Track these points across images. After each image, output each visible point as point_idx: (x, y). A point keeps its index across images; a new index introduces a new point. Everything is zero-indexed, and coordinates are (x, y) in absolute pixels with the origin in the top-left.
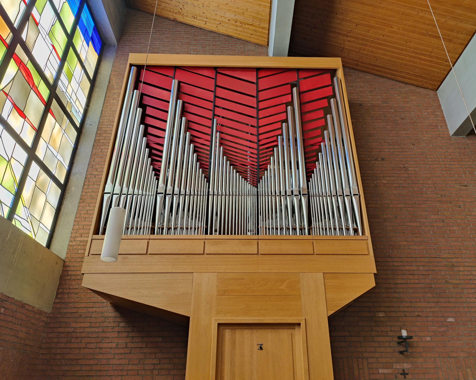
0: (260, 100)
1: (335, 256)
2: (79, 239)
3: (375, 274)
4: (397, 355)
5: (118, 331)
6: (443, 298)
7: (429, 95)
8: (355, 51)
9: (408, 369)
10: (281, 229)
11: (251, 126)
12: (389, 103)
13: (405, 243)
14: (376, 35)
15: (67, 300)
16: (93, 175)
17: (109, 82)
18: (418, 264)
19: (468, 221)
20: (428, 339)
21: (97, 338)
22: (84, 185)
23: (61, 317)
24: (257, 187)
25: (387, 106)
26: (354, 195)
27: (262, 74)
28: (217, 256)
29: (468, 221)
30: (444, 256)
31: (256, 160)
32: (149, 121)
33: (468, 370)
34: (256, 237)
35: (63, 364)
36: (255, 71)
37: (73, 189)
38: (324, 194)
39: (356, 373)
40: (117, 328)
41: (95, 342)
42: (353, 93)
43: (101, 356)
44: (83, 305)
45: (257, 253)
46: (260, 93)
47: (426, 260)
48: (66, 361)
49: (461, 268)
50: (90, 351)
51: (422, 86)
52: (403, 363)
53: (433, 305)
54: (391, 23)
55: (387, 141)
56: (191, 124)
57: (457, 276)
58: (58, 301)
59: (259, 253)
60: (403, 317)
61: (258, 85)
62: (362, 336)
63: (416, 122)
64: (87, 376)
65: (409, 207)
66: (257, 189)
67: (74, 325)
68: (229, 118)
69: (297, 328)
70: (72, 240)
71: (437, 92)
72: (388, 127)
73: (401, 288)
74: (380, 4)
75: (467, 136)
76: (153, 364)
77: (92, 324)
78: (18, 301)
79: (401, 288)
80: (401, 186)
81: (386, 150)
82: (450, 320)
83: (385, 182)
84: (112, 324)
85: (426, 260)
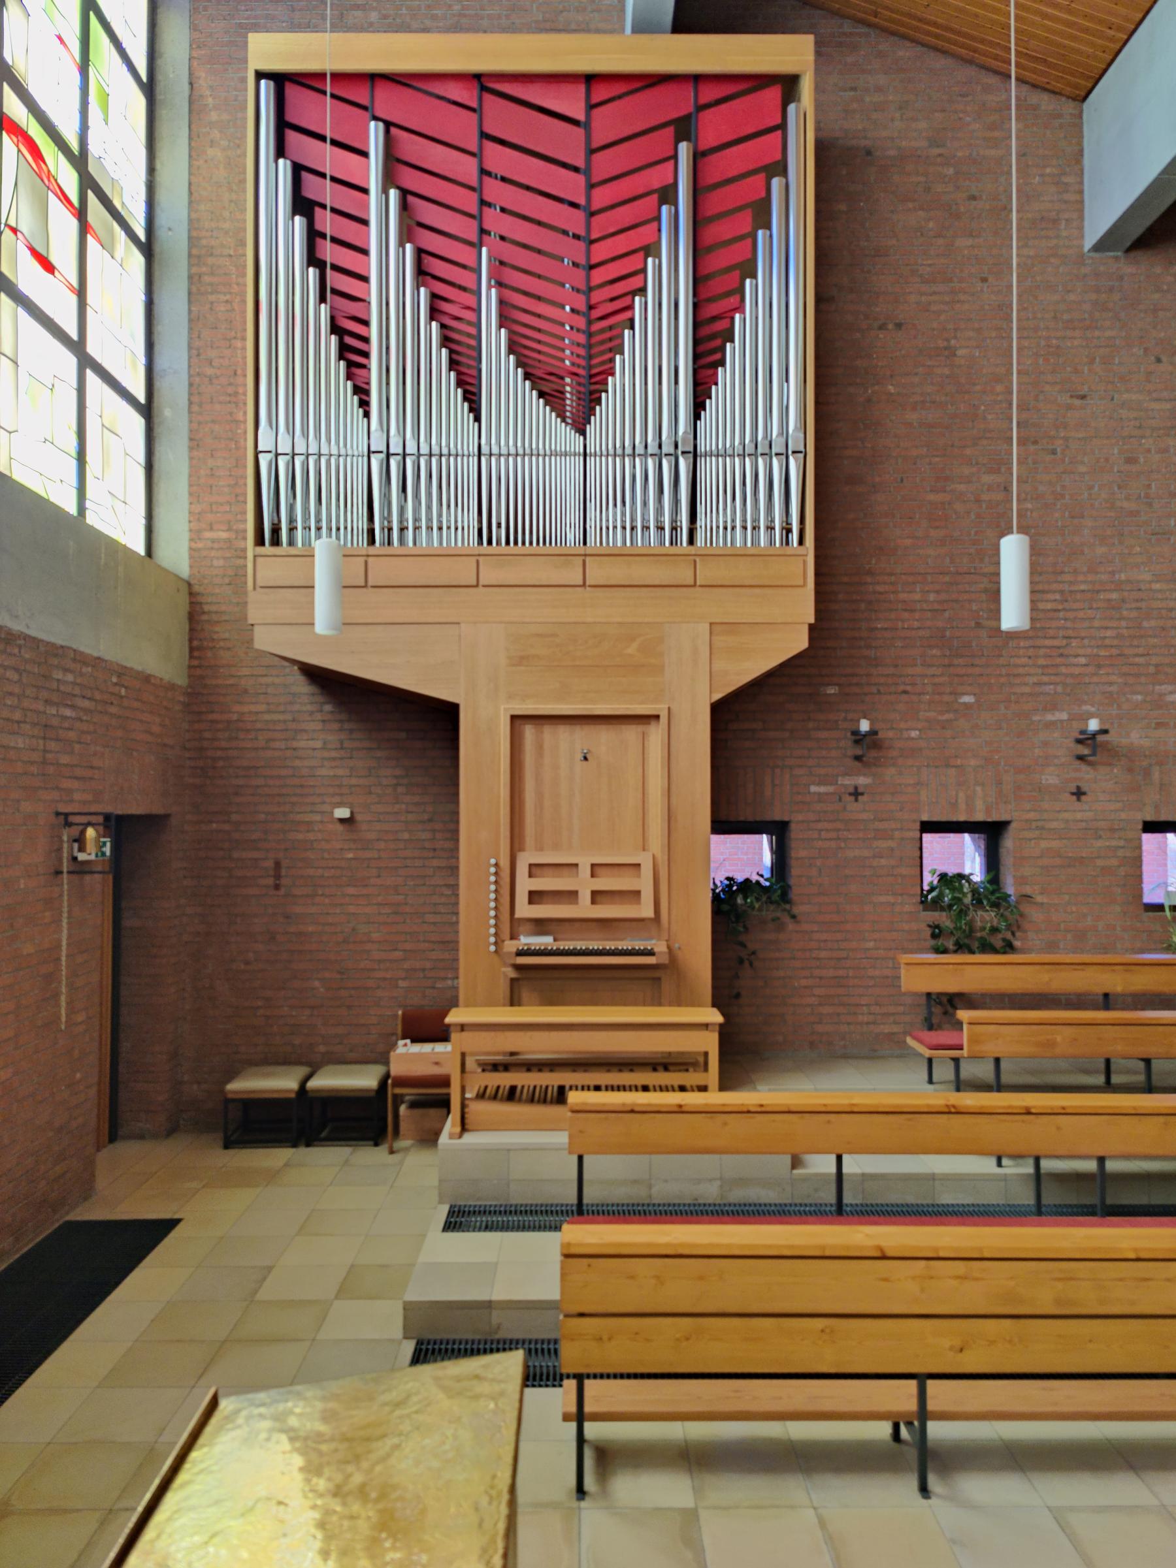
0: (595, 180)
2: (208, 535)
6: (962, 656)
7: (1060, 116)
9: (866, 786)
13: (908, 542)
16: (206, 376)
17: (191, 84)
19: (1063, 487)
20: (914, 734)
22: (191, 403)
24: (583, 432)
27: (601, 92)
29: (1063, 487)
33: (978, 789)
37: (167, 412)
39: (768, 792)
43: (297, 763)
50: (277, 754)
51: (1048, 86)
53: (939, 671)
55: (918, 270)
56: (428, 261)
58: (196, 663)
65: (937, 456)
66: (585, 439)
67: (237, 708)
69: (653, 723)
71: (1086, 105)
72: (931, 225)
75: (1129, 250)
78: (138, 673)
84: (309, 708)
85: (947, 579)
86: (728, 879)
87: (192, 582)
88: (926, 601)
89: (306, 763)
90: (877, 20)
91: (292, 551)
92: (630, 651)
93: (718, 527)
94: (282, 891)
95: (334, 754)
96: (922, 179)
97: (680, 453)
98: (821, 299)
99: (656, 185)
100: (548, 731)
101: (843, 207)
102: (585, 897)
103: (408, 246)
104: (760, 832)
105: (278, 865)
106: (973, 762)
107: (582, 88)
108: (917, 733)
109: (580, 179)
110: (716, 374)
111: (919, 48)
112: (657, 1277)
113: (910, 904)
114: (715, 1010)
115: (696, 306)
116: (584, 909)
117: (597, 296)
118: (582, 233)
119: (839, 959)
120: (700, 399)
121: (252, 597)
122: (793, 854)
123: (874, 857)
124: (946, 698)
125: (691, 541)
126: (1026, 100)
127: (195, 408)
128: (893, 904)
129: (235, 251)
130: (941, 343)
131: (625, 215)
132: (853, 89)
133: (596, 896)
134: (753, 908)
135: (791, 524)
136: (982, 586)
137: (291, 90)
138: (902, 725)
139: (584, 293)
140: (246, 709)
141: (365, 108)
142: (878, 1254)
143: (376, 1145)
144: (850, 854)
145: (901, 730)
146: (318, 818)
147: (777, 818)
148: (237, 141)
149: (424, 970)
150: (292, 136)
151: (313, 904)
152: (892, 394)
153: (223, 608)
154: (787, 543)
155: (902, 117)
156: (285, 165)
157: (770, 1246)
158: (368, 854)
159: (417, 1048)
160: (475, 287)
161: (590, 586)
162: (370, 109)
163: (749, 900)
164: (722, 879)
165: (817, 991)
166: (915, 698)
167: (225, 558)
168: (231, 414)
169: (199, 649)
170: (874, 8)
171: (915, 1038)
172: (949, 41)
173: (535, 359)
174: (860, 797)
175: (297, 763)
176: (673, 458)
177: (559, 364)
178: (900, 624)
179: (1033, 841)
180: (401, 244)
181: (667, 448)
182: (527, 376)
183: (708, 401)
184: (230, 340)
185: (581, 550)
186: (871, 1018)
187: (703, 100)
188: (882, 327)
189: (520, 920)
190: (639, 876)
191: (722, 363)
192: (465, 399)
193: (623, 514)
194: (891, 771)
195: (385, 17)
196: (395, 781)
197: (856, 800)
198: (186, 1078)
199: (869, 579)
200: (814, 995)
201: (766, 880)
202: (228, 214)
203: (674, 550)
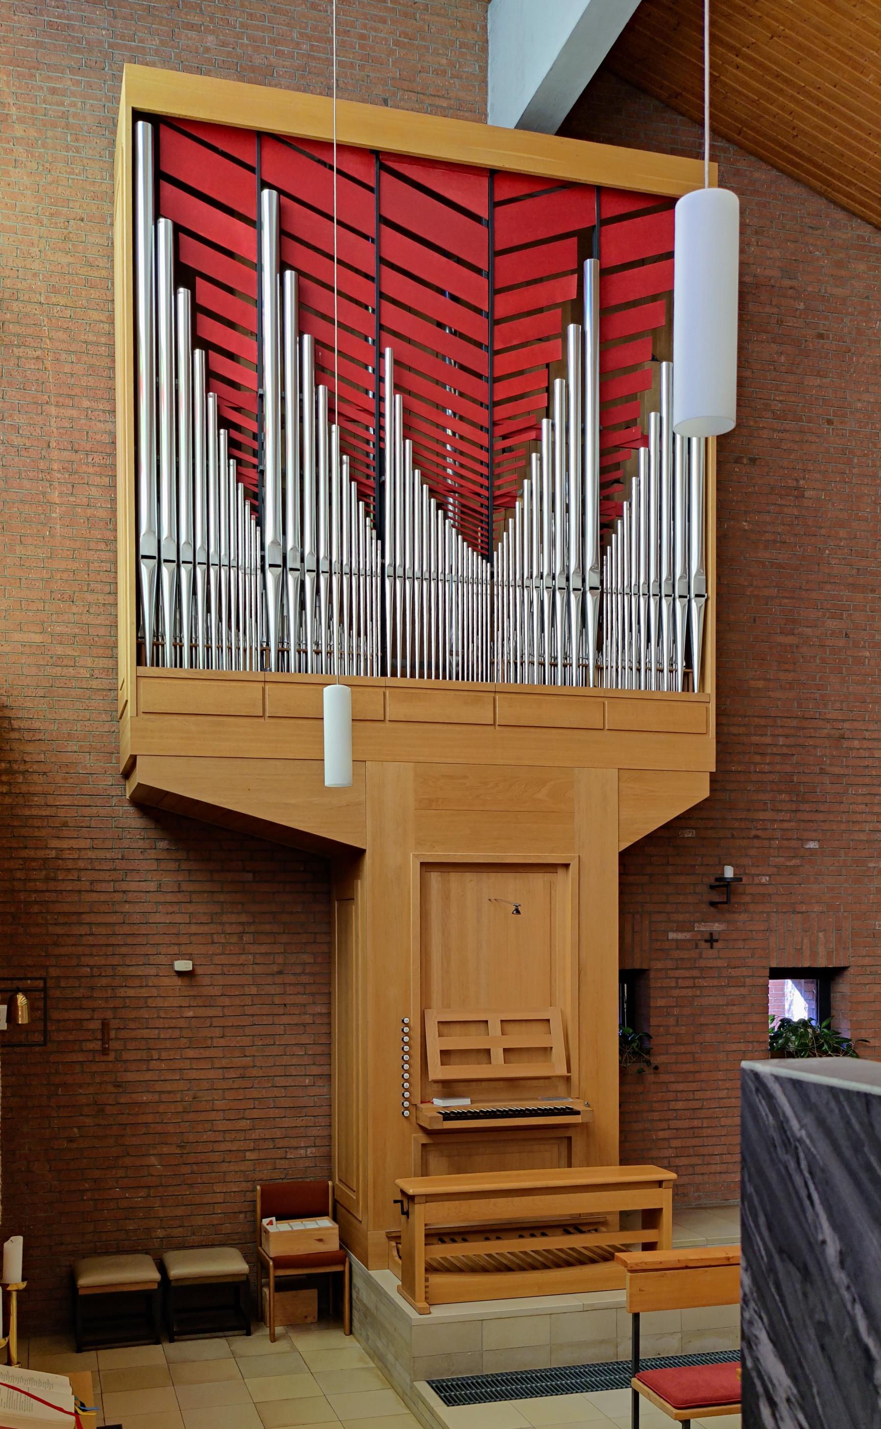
0: (498, 286)
1: (645, 734)
2: (18, 636)
3: (711, 773)
4: (705, 908)
6: (807, 802)
8: (747, 97)
9: (719, 932)
12: (796, 278)
13: (761, 684)
14: (814, 77)
15: (24, 789)
18: (776, 732)
20: (765, 879)
23: (21, 826)
24: (488, 557)
25: (791, 288)
26: (697, 596)
27: (504, 191)
30: (829, 716)
31: (486, 483)
33: (821, 935)
35: (50, 922)
36: (485, 176)
41: (111, 878)
43: (127, 908)
44: (65, 801)
45: (492, 723)
47: (795, 723)
48: (56, 917)
49: (856, 744)
50: (103, 897)
53: (787, 816)
54: (865, 63)
57: (844, 759)
62: (647, 875)
63: (850, 350)
66: (492, 566)
67: (55, 843)
69: (561, 871)
72: (783, 359)
74: (854, 8)
77: (96, 842)
80: (779, 540)
81: (765, 434)
82: (812, 845)
83: (747, 528)
84: (141, 844)
85: (795, 723)
88: (776, 745)
89: (138, 908)
90: (739, 138)
94: (111, 1057)
95: (169, 898)
96: (775, 310)
100: (454, 877)
102: (498, 1055)
105: (105, 1024)
106: (817, 908)
107: (485, 182)
108: (767, 878)
111: (774, 172)
116: (498, 1068)
123: (727, 1005)
124: (794, 844)
126: (869, 241)
129: (47, 298)
130: (791, 483)
136: (826, 731)
138: (754, 871)
140: (65, 844)
141: (252, 169)
143: (249, 1334)
144: (705, 1001)
145: (753, 875)
146: (153, 971)
149: (273, 1139)
151: (148, 1070)
152: (745, 530)
153: (37, 725)
155: (758, 243)
159: (284, 1226)
165: (675, 1143)
166: (766, 843)
167: (38, 666)
168: (44, 494)
170: (740, 126)
172: (808, 172)
174: (715, 944)
175: (127, 908)
178: (752, 768)
179: (867, 986)
180: (300, 333)
184: (41, 405)
186: (724, 1167)
187: (608, 213)
188: (738, 461)
194: (743, 917)
195: (224, 44)
196: (240, 929)
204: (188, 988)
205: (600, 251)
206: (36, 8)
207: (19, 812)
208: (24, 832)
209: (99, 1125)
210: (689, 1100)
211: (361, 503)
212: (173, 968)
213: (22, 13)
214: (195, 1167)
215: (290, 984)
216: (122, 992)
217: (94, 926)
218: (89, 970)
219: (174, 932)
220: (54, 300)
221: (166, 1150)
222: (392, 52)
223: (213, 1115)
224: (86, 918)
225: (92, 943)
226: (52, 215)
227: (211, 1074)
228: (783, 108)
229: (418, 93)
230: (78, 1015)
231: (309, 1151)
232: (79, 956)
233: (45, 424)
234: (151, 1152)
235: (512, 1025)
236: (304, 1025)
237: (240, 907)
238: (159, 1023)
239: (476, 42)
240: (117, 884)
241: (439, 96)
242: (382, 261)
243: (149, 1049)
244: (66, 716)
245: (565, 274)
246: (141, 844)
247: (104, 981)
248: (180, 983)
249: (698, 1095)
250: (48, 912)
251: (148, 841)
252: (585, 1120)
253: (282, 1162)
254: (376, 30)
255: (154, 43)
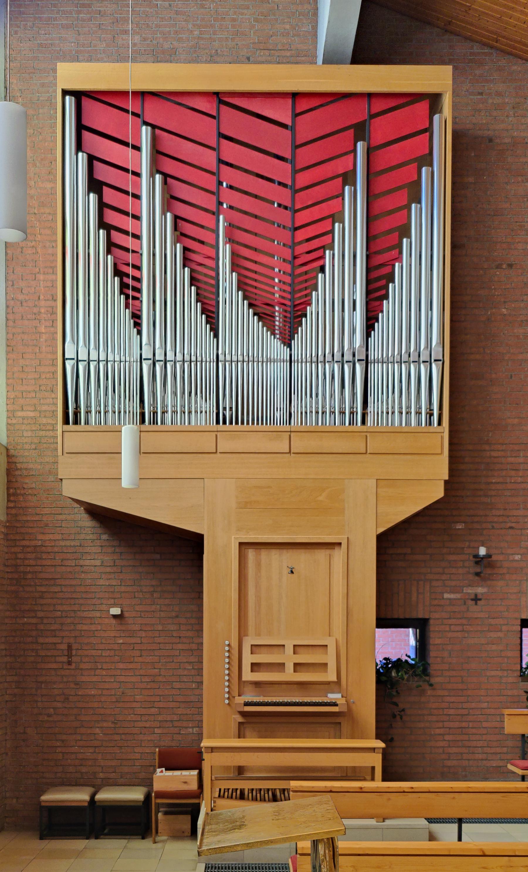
2: (20, 414)
4: (471, 577)
5: (101, 545)
9: (482, 594)
10: (323, 413)
11: (280, 183)
13: (516, 421)
15: (23, 505)
16: (18, 300)
20: (517, 557)
21: (74, 554)
22: (7, 320)
24: (290, 346)
28: (234, 455)
32: (112, 218)
34: (287, 428)
35: (38, 584)
36: (290, 98)
38: (391, 359)
39: (414, 598)
40: (99, 541)
42: (480, 111)
46: (298, 151)
50: (69, 569)
52: (476, 586)
55: (524, 226)
58: (12, 505)
59: (292, 452)
60: (489, 529)
61: (295, 130)
64: (71, 598)
66: (291, 350)
67: (40, 537)
68: (238, 146)
69: (337, 549)
70: (11, 415)
73: (494, 490)
76: (152, 585)
79: (494, 490)
81: (520, 246)
83: (505, 313)
84: (91, 536)
86: (385, 659)
87: (9, 448)
91: (88, 428)
92: (320, 498)
93: (382, 412)
94: (73, 666)
95: (108, 570)
97: (356, 361)
98: (454, 246)
99: (341, 171)
100: (264, 553)
101: (471, 179)
102: (290, 667)
103: (169, 215)
104: (407, 627)
105: (70, 647)
109: (288, 167)
110: (382, 305)
112: (353, 866)
113: (513, 677)
114: (379, 741)
115: (368, 257)
117: (300, 249)
118: (289, 205)
119: (462, 715)
120: (371, 322)
121: (61, 459)
122: (432, 641)
125: (363, 422)
127: (11, 323)
128: (501, 677)
131: (318, 192)
132: (481, 94)
133: (297, 666)
134: (403, 679)
135: (433, 410)
137: (86, 103)
139: (290, 247)
140: (47, 537)
142: (481, 854)
143: (143, 838)
146: (98, 614)
147: (421, 616)
148: (40, 130)
149: (172, 721)
150: (86, 134)
153: (31, 466)
154: (430, 424)
155: (514, 114)
156: (83, 156)
157: (418, 849)
158: (133, 640)
160: (213, 243)
161: (293, 453)
162: (141, 117)
163: (400, 674)
164: (381, 659)
165: (447, 737)
169: (14, 495)
170: (495, 37)
171: (512, 764)
173: (253, 293)
174: (479, 602)
176: (351, 364)
177: (272, 297)
178: (508, 480)
180: (164, 213)
181: (348, 357)
182: (250, 305)
183: (376, 324)
185: (287, 428)
187: (375, 110)
188: (499, 267)
189: (245, 682)
190: (326, 653)
191: (386, 297)
192: (207, 322)
193: (317, 403)
194: (501, 583)
195: (145, 39)
196: (152, 589)
197: (476, 604)
198: (8, 795)
199: (487, 447)
200: (445, 740)
201: (412, 660)
202: (33, 183)
203: (352, 428)
204: (119, 625)
205: (370, 138)
206: (33, 37)
207: (20, 518)
208: (23, 530)
209: (66, 707)
210: (459, 709)
211: (255, 317)
212: (109, 613)
213: (25, 41)
214: (123, 737)
215: (183, 624)
216: (79, 627)
217: (63, 587)
218: (60, 613)
219: (111, 591)
220: (42, 211)
221: (105, 724)
222: (254, 26)
223: (134, 705)
224: (59, 582)
225: (62, 597)
226: (42, 160)
227: (133, 679)
228: (518, 19)
229: (270, 50)
230: (54, 640)
231: (195, 729)
232: (54, 605)
233: (37, 286)
234: (96, 725)
235: (302, 648)
236: (192, 650)
237: (152, 575)
238: (102, 647)
239: (310, 10)
240: (77, 561)
241: (284, 50)
242: (221, 161)
243: (96, 662)
244: (48, 460)
245: (346, 154)
246: (91, 536)
247: (69, 620)
248: (114, 622)
249: (465, 705)
250: (36, 578)
251: (95, 535)
252: (341, 710)
253: (178, 736)
254: (242, 14)
255: (102, 46)
